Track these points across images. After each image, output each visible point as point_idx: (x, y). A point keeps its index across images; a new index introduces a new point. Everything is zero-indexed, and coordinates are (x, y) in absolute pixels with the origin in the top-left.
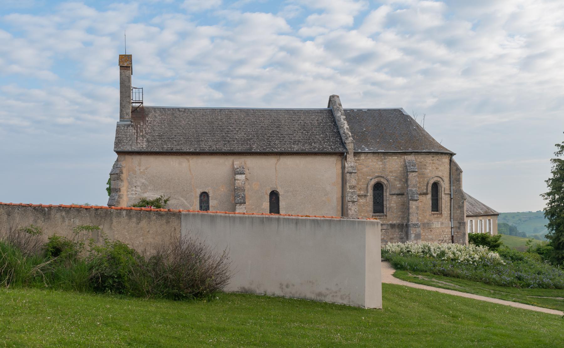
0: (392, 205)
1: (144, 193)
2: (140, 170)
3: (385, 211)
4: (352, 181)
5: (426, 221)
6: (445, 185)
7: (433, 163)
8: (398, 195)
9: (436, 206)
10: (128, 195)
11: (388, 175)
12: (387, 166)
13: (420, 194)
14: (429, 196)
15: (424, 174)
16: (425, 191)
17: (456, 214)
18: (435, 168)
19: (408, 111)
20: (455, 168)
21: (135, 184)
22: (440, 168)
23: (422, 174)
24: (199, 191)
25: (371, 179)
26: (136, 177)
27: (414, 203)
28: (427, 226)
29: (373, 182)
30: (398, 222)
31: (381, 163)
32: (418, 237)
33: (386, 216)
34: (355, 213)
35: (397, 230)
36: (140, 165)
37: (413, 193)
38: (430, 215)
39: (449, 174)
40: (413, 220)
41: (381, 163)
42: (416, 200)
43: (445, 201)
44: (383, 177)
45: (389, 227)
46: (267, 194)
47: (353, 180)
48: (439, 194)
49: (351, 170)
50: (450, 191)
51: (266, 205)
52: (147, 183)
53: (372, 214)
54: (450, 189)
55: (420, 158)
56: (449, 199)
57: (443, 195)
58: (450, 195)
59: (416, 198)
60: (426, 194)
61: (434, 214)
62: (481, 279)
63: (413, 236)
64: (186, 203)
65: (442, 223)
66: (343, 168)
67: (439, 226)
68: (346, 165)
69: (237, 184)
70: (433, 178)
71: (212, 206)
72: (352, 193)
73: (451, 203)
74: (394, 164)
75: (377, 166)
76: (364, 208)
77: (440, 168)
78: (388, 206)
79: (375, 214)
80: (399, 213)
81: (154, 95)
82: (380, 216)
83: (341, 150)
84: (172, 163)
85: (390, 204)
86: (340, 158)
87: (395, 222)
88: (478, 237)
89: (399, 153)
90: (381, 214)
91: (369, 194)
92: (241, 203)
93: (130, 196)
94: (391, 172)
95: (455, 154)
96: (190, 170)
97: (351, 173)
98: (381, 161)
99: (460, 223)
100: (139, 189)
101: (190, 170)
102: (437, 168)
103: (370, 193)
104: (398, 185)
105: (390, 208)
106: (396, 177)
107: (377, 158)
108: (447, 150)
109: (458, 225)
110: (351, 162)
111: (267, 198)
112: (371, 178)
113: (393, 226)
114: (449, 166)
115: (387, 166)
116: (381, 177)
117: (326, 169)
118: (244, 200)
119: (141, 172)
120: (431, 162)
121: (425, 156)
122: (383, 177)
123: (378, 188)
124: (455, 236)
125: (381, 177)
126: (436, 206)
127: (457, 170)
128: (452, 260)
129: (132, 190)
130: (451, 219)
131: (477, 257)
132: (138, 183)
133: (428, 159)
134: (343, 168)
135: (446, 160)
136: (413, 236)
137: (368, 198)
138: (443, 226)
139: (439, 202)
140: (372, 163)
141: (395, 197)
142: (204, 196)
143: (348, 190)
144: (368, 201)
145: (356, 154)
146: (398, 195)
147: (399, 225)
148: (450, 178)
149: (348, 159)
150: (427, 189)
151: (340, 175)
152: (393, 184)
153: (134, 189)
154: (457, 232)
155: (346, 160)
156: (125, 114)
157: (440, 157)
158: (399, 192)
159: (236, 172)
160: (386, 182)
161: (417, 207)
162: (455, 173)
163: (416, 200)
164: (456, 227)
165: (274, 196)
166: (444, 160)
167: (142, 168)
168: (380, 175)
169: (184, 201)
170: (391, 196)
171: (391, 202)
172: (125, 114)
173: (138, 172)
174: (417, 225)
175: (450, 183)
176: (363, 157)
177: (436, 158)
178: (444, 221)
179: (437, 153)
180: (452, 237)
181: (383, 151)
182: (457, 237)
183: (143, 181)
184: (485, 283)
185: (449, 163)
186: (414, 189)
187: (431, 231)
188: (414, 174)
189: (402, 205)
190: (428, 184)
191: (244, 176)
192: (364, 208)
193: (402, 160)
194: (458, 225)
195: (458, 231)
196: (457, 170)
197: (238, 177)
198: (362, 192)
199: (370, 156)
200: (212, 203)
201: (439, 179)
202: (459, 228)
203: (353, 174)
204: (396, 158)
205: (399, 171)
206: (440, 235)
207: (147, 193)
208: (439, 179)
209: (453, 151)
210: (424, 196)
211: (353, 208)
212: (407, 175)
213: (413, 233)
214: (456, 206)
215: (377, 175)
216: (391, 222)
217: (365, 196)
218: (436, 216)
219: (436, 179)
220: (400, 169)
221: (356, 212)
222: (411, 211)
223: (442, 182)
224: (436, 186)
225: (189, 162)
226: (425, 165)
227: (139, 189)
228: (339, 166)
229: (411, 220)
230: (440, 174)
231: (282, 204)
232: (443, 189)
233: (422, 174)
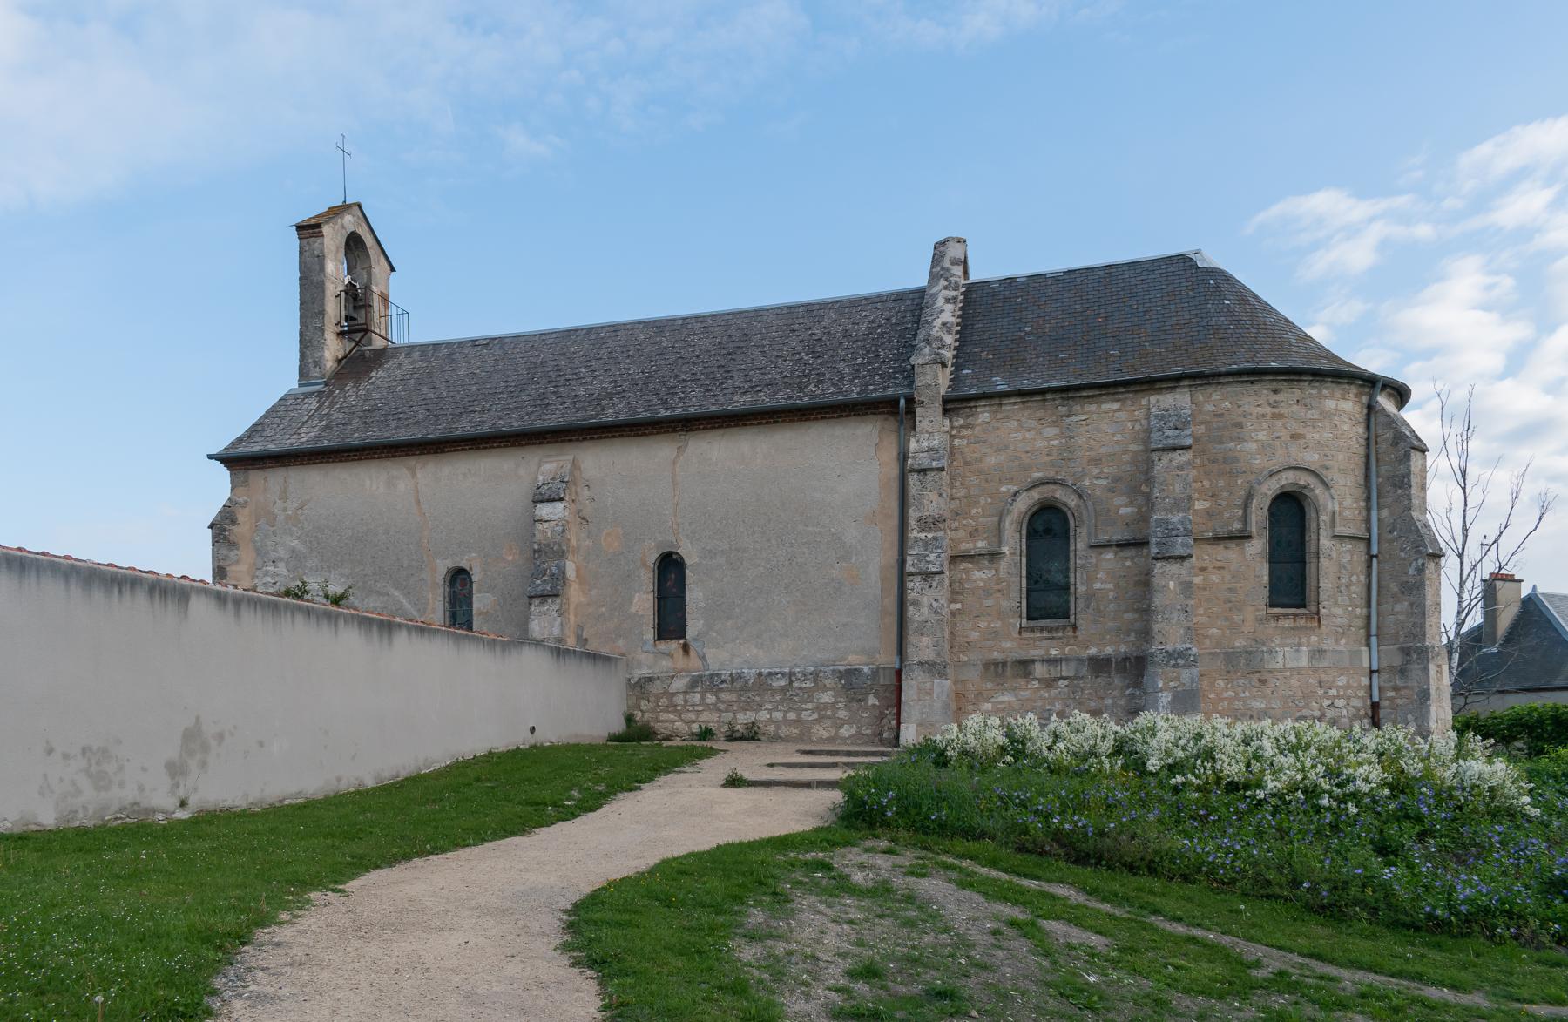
0: (1097, 586)
2: (285, 510)
4: (930, 500)
5: (1239, 643)
6: (1339, 503)
7: (1279, 416)
8: (1122, 545)
9: (1291, 585)
11: (1084, 474)
12: (1081, 440)
13: (1217, 539)
14: (1257, 546)
15: (1235, 460)
16: (1237, 526)
17: (1390, 619)
18: (1285, 435)
19: (1213, 257)
20: (1389, 435)
21: (273, 555)
22: (1313, 436)
23: (1225, 461)
24: (443, 566)
25: (1015, 494)
26: (274, 533)
27: (1174, 568)
28: (1245, 664)
29: (1024, 504)
30: (1123, 648)
32: (1185, 702)
33: (1075, 627)
34: (933, 618)
35: (1117, 681)
37: (1171, 533)
38: (1260, 621)
39: (1361, 461)
40: (1169, 635)
41: (1056, 431)
42: (1182, 558)
43: (1336, 566)
44: (1063, 484)
45: (1084, 670)
46: (644, 564)
47: (934, 496)
48: (1311, 537)
49: (924, 460)
50: (1369, 530)
51: (644, 602)
53: (1016, 622)
54: (1368, 520)
55: (1216, 400)
56: (1364, 558)
57: (1325, 542)
58: (1368, 541)
59: (1179, 551)
60: (1243, 537)
61: (1277, 617)
62: (1295, 883)
63: (1165, 698)
64: (407, 606)
65: (1317, 653)
66: (903, 456)
67: (1304, 662)
68: (913, 445)
69: (539, 536)
70: (1272, 474)
71: (481, 613)
72: (926, 543)
73: (1369, 575)
74: (1108, 428)
75: (1040, 444)
76: (989, 603)
77: (1313, 436)
78: (1081, 589)
79: (1032, 624)
80: (1129, 616)
81: (426, 308)
82: (1050, 629)
85: (1089, 581)
86: (891, 424)
87: (1109, 650)
88: (1541, 721)
90: (1062, 622)
91: (1005, 550)
92: (544, 597)
94: (1095, 462)
96: (418, 502)
97: (923, 471)
98: (1055, 424)
99: (1406, 652)
101: (418, 502)
102: (1295, 437)
103: (1013, 544)
104: (1123, 511)
105: (1090, 597)
106: (1116, 479)
107: (1040, 414)
109: (1397, 660)
110: (930, 432)
112: (1014, 488)
113: (1099, 665)
114: (1361, 430)
115: (1081, 440)
116: (1055, 482)
117: (844, 466)
119: (288, 517)
120: (1269, 410)
121: (1235, 388)
122: (1063, 484)
123: (1048, 527)
124: (1385, 703)
125: (1055, 482)
126: (1291, 585)
127: (1395, 444)
128: (1233, 787)
129: (266, 574)
130: (1368, 636)
131: (1368, 775)
132: (282, 553)
133: (1254, 401)
134: (903, 456)
135: (1345, 406)
136: (1165, 698)
137: (1003, 564)
138: (1325, 664)
139: (1311, 569)
140: (1019, 435)
141: (1109, 555)
142: (459, 577)
143: (915, 534)
144: (1002, 574)
145: (952, 405)
146: (1122, 545)
147: (1126, 659)
148: (1367, 477)
149: (922, 424)
150: (1245, 519)
152: (1102, 506)
154: (1396, 689)
155: (914, 428)
157: (1310, 391)
158: (1127, 536)
160: (1072, 501)
161: (1187, 587)
162: (1391, 458)
163: (1182, 558)
164: (1391, 669)
166: (1330, 404)
168: (1051, 474)
169: (401, 598)
170: (1093, 553)
171: (1096, 575)
173: (281, 518)
174: (1182, 654)
175: (1368, 499)
176: (984, 415)
177: (1289, 396)
178: (1329, 645)
179: (1293, 375)
180: (1375, 707)
182: (1395, 708)
184: (1309, 908)
185: (1361, 417)
186: (1176, 518)
187: (1263, 682)
188: (1179, 458)
189: (1137, 583)
190: (1249, 497)
191: (560, 506)
192: (989, 603)
193: (1140, 413)
194: (1397, 660)
195: (1400, 683)
196: (1395, 444)
197: (544, 510)
198: (981, 544)
199: (1011, 407)
200: (481, 601)
201: (1304, 479)
202: (1403, 672)
203: (930, 475)
204: (1116, 406)
205: (1126, 458)
206: (1305, 696)
208: (1304, 479)
210: (1232, 545)
211: (925, 600)
212: (1150, 465)
213: (1163, 683)
214: (1394, 588)
215: (1037, 475)
216: (1093, 651)
217: (994, 556)
218: (1288, 623)
219: (1287, 479)
220: (1134, 448)
221: (936, 612)
222: (1158, 600)
223: (1319, 491)
224: (1291, 511)
225: (414, 475)
226: (1239, 425)
228: (890, 453)
229: (1159, 638)
230: (1311, 458)
231: (695, 596)
232: (1324, 518)
233: (1225, 461)
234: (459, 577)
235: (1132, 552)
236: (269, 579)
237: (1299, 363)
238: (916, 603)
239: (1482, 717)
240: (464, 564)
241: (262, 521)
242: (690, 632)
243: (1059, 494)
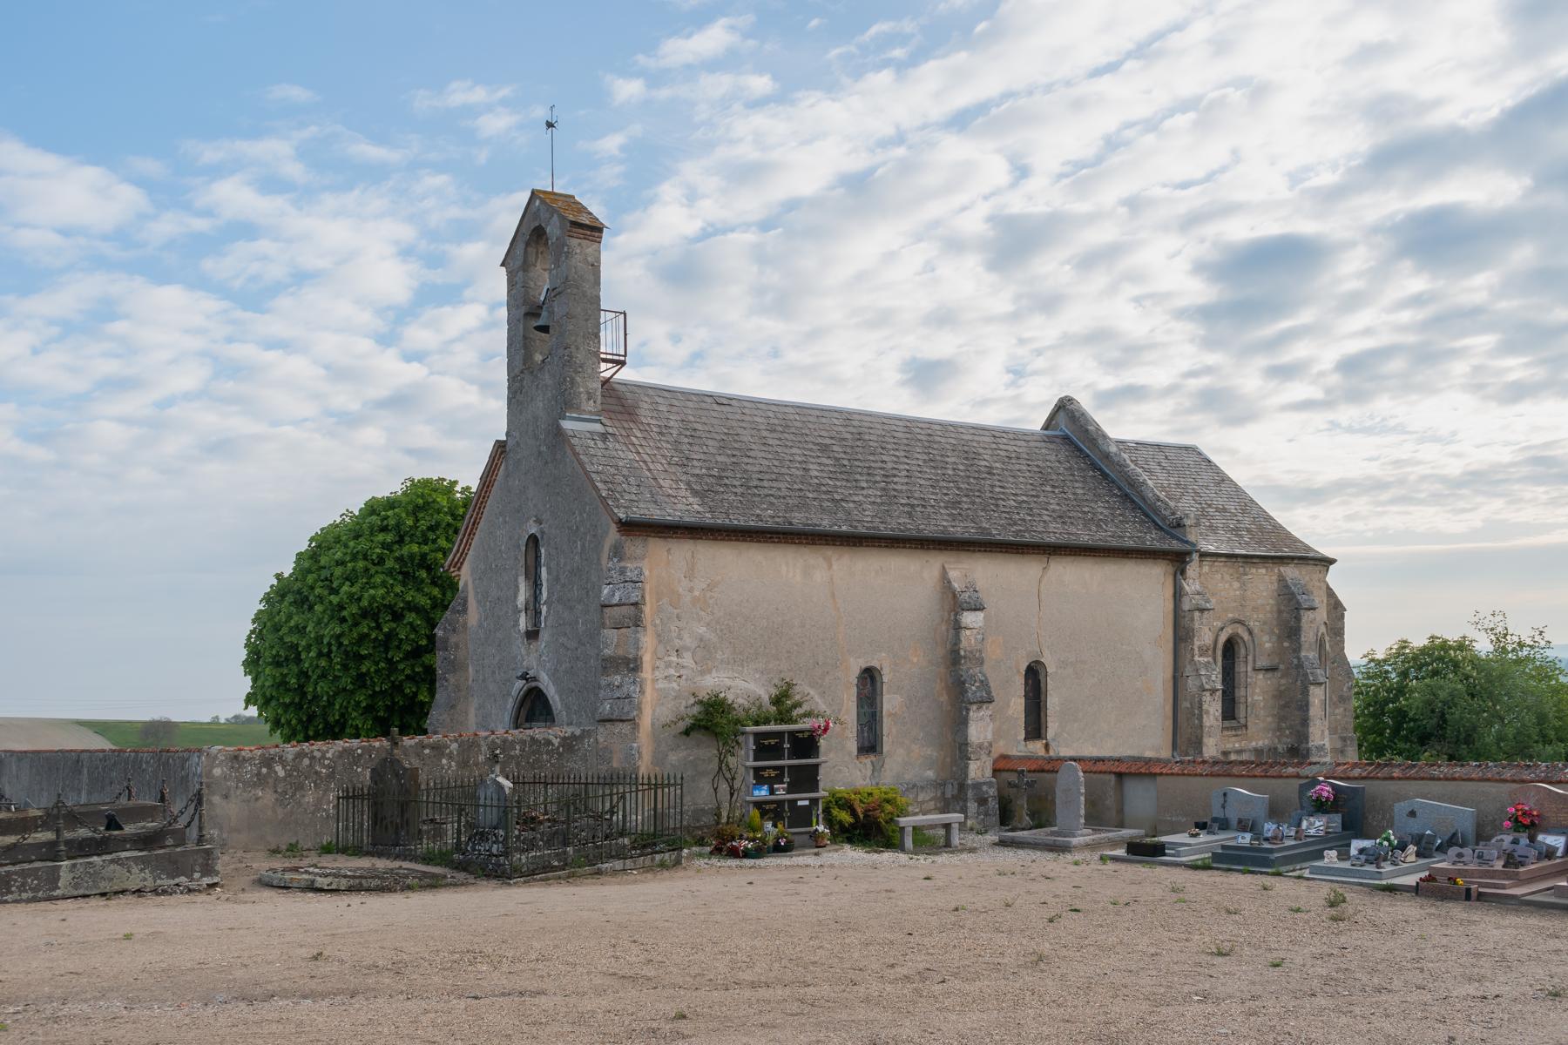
1: (702, 673)
2: (691, 590)
3: (1242, 714)
8: (1267, 670)
10: (655, 681)
24: (855, 666)
31: (1236, 585)
36: (690, 574)
49: (1198, 600)
52: (711, 636)
71: (890, 715)
83: (1176, 545)
84: (784, 568)
87: (1260, 743)
89: (1272, 558)
93: (661, 685)
94: (1255, 609)
95: (1332, 561)
96: (833, 595)
98: (1238, 579)
100: (687, 660)
101: (833, 595)
108: (1309, 549)
109: (1339, 745)
111: (1019, 682)
118: (989, 693)
129: (668, 665)
132: (688, 641)
134: (1178, 594)
142: (870, 677)
146: (1267, 670)
151: (1171, 616)
153: (674, 659)
156: (584, 397)
159: (956, 604)
160: (1246, 637)
165: (1034, 677)
167: (699, 584)
172: (584, 397)
181: (1243, 552)
183: (702, 630)
191: (981, 615)
194: (1339, 745)
197: (968, 618)
207: (714, 674)
209: (1327, 552)
225: (830, 567)
227: (687, 660)
231: (1053, 702)
234: (870, 677)
235: (1269, 675)
236: (672, 671)
237: (1286, 552)
238: (1207, 712)
239: (222, 721)
240: (875, 664)
241: (665, 600)
242: (1050, 734)
243: (1241, 631)
